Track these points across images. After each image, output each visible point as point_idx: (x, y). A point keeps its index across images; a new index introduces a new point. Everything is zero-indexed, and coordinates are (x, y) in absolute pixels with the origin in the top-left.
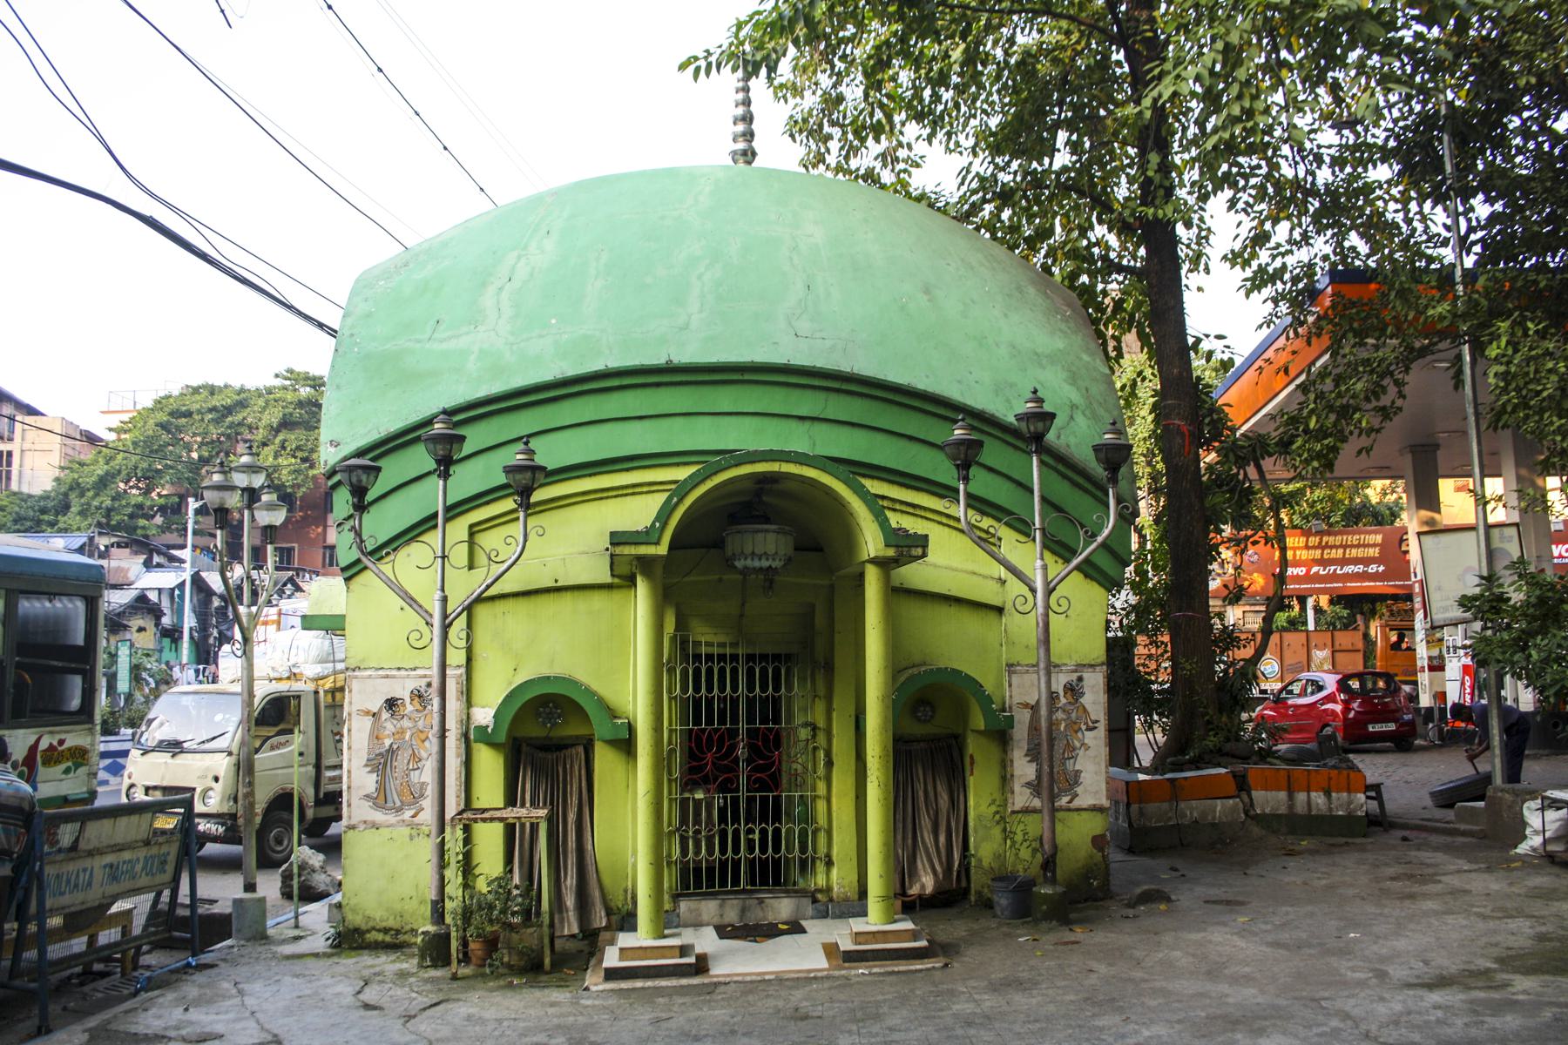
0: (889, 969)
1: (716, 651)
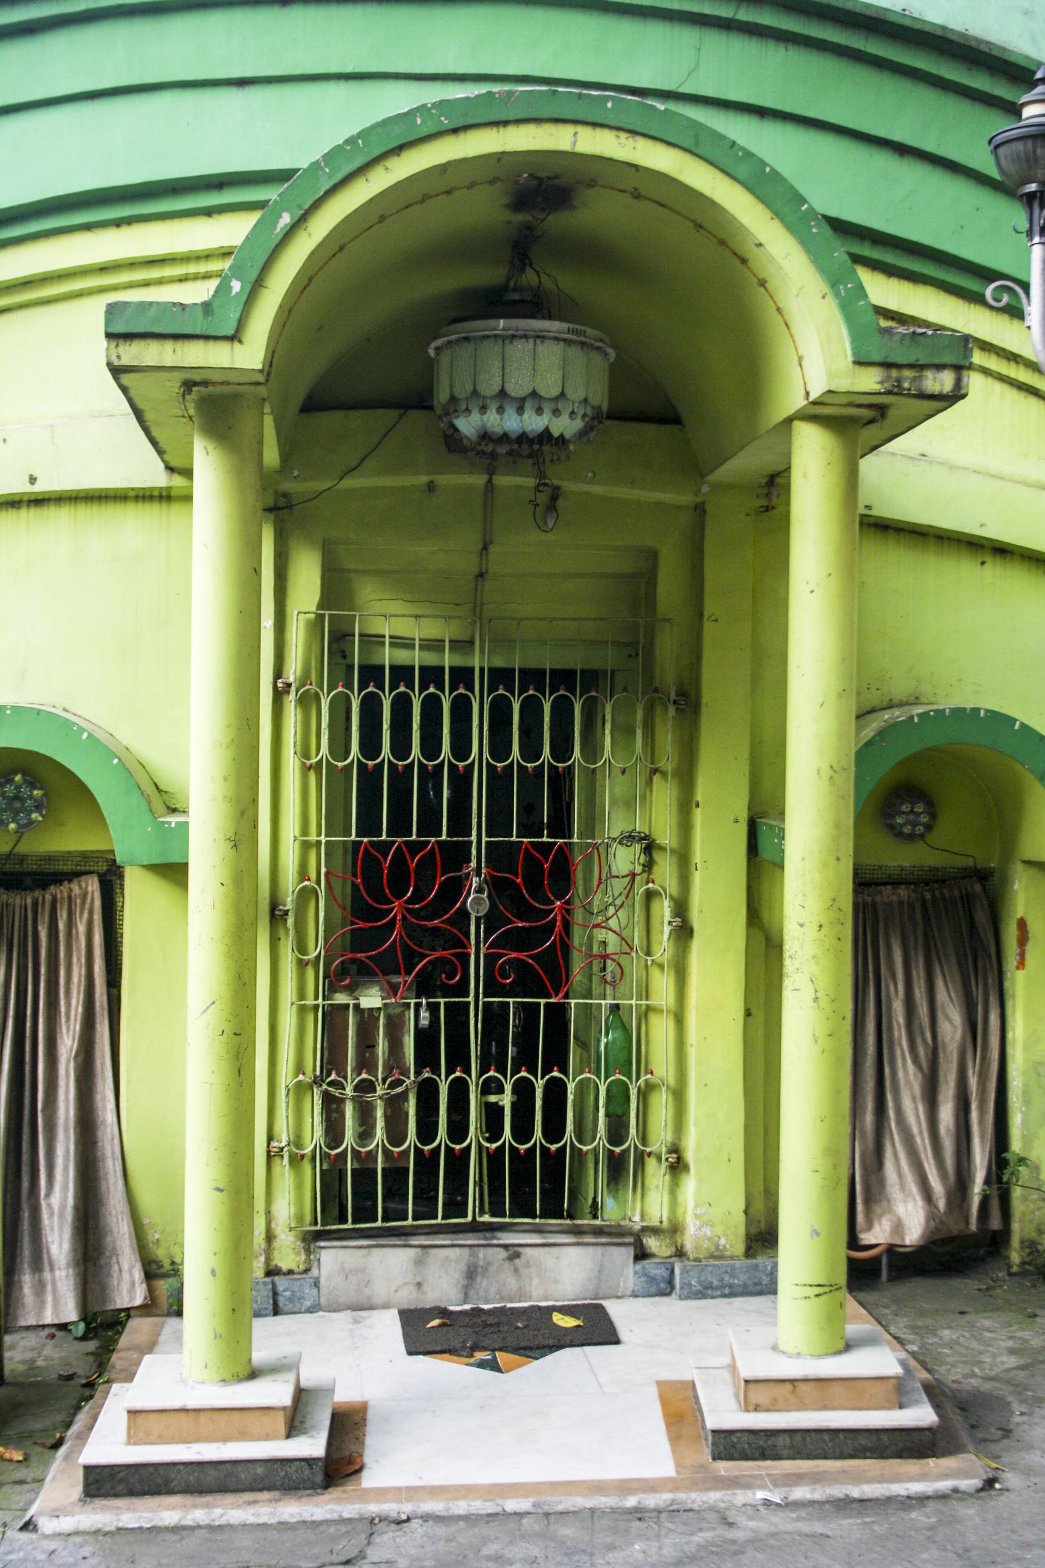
0: (837, 1491)
1: (416, 658)
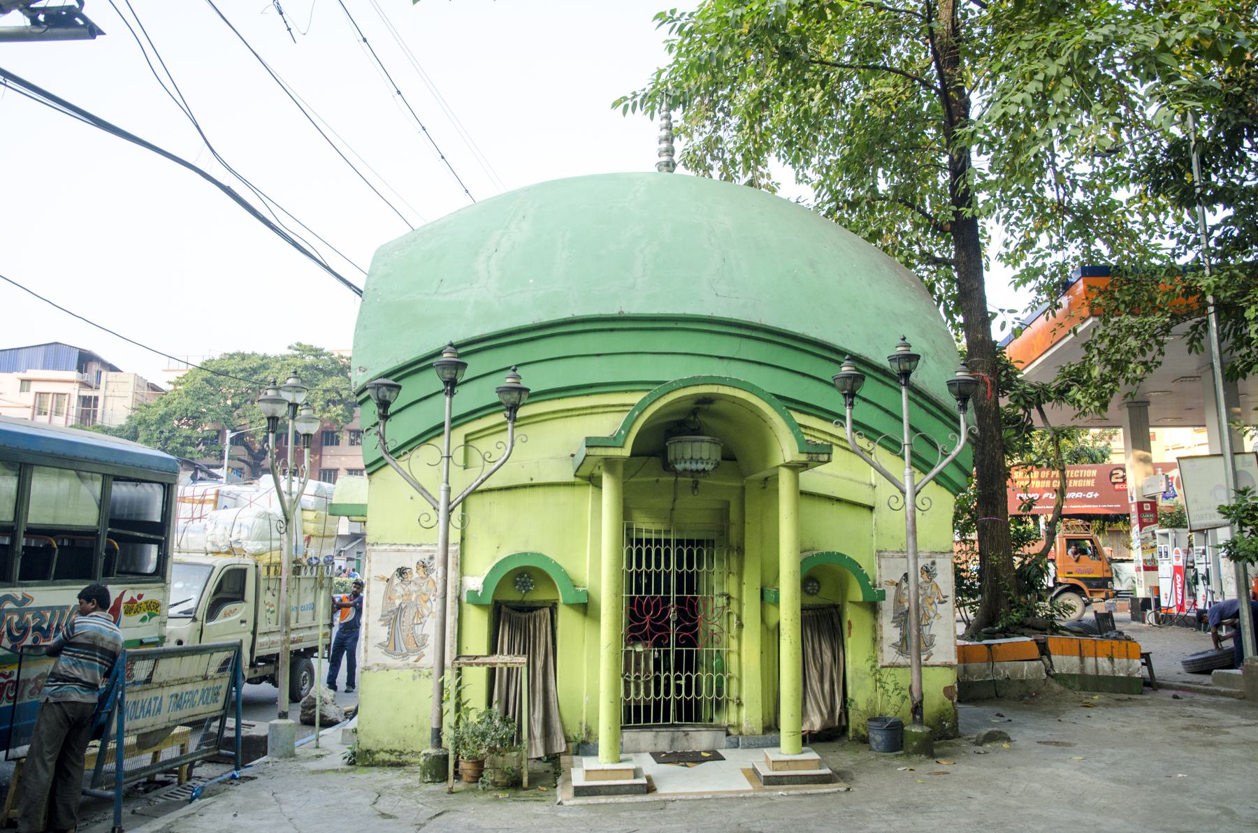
0: (803, 792)
1: (654, 536)
